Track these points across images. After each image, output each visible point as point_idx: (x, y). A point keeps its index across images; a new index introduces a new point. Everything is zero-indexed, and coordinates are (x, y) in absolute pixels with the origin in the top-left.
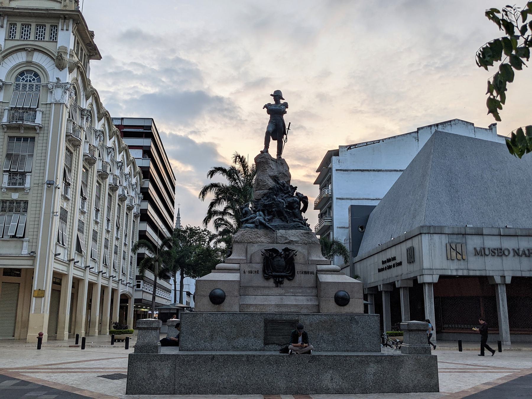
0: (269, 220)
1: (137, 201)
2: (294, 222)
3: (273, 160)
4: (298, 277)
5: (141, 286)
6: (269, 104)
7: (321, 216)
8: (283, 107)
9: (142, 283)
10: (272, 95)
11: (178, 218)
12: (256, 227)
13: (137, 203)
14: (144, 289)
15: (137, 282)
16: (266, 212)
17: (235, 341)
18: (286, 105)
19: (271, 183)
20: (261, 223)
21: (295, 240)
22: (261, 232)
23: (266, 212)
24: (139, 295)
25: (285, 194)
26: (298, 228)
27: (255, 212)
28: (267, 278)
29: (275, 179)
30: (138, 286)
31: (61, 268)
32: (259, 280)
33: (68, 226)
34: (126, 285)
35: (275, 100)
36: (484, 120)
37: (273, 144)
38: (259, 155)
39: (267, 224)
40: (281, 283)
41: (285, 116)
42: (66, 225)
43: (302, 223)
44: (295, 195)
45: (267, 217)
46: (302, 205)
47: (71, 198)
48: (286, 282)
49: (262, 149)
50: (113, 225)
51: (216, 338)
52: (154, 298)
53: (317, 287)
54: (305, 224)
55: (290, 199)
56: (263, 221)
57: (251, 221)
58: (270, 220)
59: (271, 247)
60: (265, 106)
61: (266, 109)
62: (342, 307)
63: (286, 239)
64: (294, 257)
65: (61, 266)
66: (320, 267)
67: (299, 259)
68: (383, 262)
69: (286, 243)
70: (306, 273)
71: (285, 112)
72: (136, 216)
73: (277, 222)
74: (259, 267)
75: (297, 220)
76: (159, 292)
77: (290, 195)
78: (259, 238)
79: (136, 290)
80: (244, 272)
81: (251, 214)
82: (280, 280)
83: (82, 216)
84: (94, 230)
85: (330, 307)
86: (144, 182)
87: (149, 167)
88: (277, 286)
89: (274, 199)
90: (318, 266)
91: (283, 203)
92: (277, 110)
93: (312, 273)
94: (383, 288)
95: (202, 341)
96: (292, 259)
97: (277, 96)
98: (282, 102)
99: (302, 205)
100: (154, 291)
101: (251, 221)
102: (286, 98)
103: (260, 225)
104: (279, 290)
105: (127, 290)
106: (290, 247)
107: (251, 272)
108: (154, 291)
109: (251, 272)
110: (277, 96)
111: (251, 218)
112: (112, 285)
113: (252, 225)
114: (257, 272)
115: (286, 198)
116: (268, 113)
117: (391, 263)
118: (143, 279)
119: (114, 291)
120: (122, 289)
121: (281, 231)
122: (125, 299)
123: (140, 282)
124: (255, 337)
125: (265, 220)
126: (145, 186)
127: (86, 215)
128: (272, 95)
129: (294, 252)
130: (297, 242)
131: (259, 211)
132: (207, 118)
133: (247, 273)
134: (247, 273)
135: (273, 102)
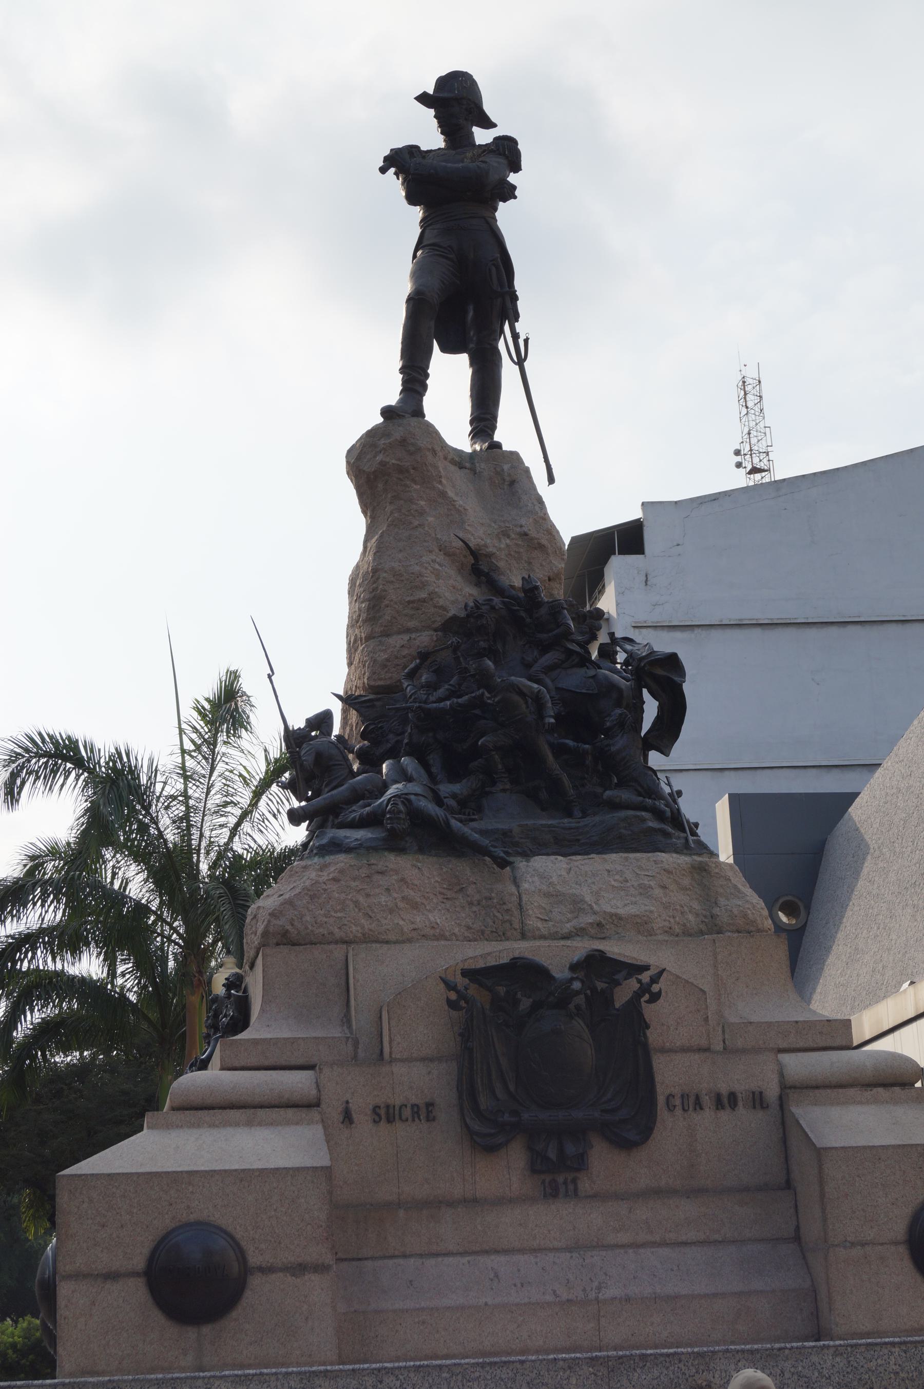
0: (463, 803)
2: (615, 806)
3: (458, 459)
4: (670, 1129)
6: (413, 150)
8: (494, 161)
10: (424, 99)
12: (394, 843)
18: (508, 152)
19: (454, 593)
20: (418, 819)
21: (632, 910)
22: (417, 872)
23: (434, 759)
25: (545, 649)
26: (647, 842)
27: (370, 761)
28: (485, 1139)
29: (478, 566)
35: (447, 125)
36: (639, 977)
37: (450, 373)
38: (372, 434)
39: (455, 823)
40: (580, 1164)
41: (506, 215)
44: (594, 655)
45: (445, 789)
46: (651, 708)
48: (604, 1164)
53: (788, 1185)
54: (677, 820)
55: (574, 679)
56: (427, 806)
57: (357, 811)
58: (470, 806)
59: (497, 952)
63: (577, 905)
64: (649, 1011)
66: (798, 1065)
67: (668, 1021)
70: (726, 1101)
71: (509, 193)
73: (506, 814)
74: (420, 1077)
75: (625, 795)
77: (570, 653)
78: (415, 906)
80: (348, 1117)
81: (353, 775)
82: (570, 1149)
88: (552, 1193)
89: (484, 680)
90: (786, 1058)
91: (336, 912)
92: (458, 180)
93: (758, 1100)
96: (633, 1021)
97: (455, 100)
98: (482, 137)
99: (651, 708)
101: (357, 811)
102: (504, 112)
104: (554, 1220)
107: (386, 1114)
109: (386, 1114)
110: (455, 100)
111: (357, 796)
114: (425, 1112)
121: (540, 863)
128: (424, 99)
129: (645, 977)
131: (393, 754)
133: (363, 1120)
134: (363, 1120)
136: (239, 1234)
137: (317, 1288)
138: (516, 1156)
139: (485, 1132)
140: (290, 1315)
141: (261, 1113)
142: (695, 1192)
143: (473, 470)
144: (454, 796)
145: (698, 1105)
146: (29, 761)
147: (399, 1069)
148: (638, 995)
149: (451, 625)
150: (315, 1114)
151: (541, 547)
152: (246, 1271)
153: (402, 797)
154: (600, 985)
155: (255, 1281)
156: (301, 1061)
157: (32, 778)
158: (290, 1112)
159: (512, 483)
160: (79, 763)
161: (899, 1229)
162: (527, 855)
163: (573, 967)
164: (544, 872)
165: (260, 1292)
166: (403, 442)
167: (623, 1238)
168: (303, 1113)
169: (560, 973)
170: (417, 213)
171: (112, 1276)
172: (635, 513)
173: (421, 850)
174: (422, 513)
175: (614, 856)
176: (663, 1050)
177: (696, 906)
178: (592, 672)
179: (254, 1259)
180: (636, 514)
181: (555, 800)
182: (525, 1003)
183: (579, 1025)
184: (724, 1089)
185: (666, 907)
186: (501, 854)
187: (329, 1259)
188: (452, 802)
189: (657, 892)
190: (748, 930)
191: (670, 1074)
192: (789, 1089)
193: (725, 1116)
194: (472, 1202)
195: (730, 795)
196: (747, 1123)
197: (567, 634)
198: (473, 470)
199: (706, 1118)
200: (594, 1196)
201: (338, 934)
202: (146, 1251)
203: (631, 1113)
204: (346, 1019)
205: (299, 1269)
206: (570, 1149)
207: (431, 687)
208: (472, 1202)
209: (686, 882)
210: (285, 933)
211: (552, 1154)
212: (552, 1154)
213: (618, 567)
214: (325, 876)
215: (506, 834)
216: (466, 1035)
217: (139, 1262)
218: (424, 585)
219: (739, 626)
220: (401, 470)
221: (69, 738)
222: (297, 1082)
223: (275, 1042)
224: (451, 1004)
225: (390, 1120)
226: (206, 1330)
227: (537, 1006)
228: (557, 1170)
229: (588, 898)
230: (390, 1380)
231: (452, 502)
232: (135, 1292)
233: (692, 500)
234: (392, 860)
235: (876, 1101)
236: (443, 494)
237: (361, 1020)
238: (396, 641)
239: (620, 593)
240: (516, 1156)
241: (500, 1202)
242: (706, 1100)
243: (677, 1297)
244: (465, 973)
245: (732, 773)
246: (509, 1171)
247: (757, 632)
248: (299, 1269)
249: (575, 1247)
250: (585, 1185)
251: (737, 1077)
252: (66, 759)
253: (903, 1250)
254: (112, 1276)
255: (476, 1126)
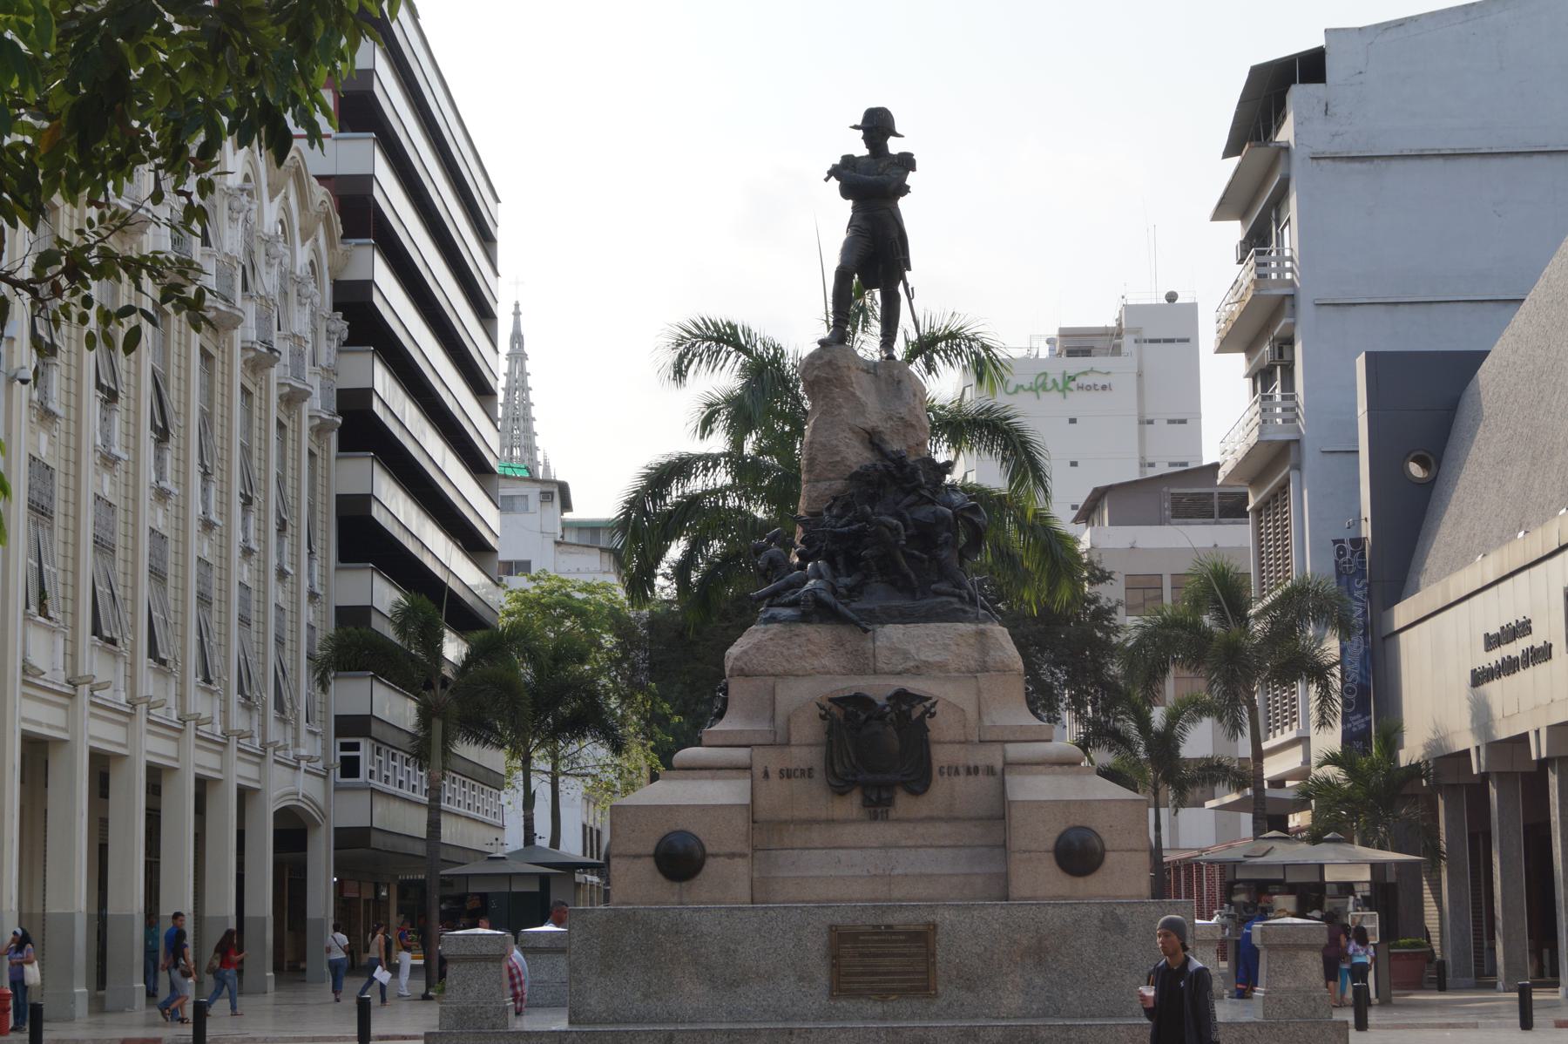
1: (327, 351)
2: (938, 594)
4: (940, 787)
5: (364, 767)
6: (848, 161)
7: (1262, 377)
9: (365, 751)
11: (517, 337)
12: (805, 618)
13: (319, 361)
14: (375, 783)
15: (344, 747)
16: (840, 559)
17: (740, 991)
18: (906, 162)
19: (857, 456)
20: (819, 603)
21: (938, 658)
22: (818, 635)
23: (840, 559)
24: (352, 812)
29: (873, 440)
30: (350, 767)
31: (45, 718)
32: (812, 798)
33: (59, 533)
34: (297, 768)
35: (868, 140)
39: (840, 607)
40: (890, 802)
41: (903, 203)
42: (51, 529)
43: (961, 598)
45: (844, 580)
47: (61, 411)
48: (903, 803)
49: (824, 333)
50: (225, 493)
51: (680, 983)
52: (434, 826)
55: (923, 513)
56: (826, 596)
58: (854, 592)
60: (835, 172)
61: (835, 183)
62: (1080, 881)
63: (906, 655)
65: (45, 707)
66: (1015, 751)
67: (942, 727)
68: (1492, 642)
69: (907, 671)
70: (973, 771)
72: (319, 430)
73: (878, 597)
74: (805, 754)
75: (944, 586)
76: (455, 794)
77: (922, 496)
78: (815, 655)
79: (338, 788)
80: (766, 775)
82: (885, 795)
83: (107, 478)
84: (152, 531)
85: (1040, 877)
86: (347, 257)
87: (368, 180)
88: (874, 818)
90: (1009, 747)
91: (897, 528)
93: (990, 771)
94: (1487, 760)
95: (638, 995)
96: (920, 729)
97: (877, 125)
100: (435, 793)
103: (818, 611)
105: (305, 788)
106: (915, 685)
107: (786, 774)
108: (435, 793)
109: (786, 774)
110: (877, 125)
112: (241, 772)
113: (788, 612)
115: (908, 507)
116: (846, 192)
117: (1515, 649)
118: (367, 734)
119: (244, 795)
120: (282, 787)
122: (292, 832)
123: (356, 747)
124: (801, 979)
125: (835, 592)
126: (354, 274)
127: (121, 466)
128: (855, 127)
129: (928, 704)
130: (942, 667)
132: (589, 739)
133: (774, 776)
134: (774, 776)
135: (861, 150)
136: (701, 837)
137: (741, 866)
138: (855, 798)
139: (840, 786)
140: (726, 880)
141: (720, 773)
142: (951, 819)
143: (875, 374)
144: (846, 586)
145: (957, 772)
146: (693, 345)
147: (795, 750)
148: (923, 714)
149: (855, 477)
150: (748, 774)
151: (913, 426)
152: (704, 856)
153: (813, 591)
154: (904, 707)
155: (710, 861)
156: (744, 742)
157: (697, 360)
158: (734, 773)
159: (899, 382)
160: (739, 347)
161: (1051, 844)
162: (883, 623)
163: (889, 699)
164: (892, 635)
165: (711, 866)
166: (830, 363)
167: (910, 843)
168: (741, 773)
169: (881, 702)
170: (850, 203)
171: (638, 856)
172: (1316, 41)
173: (821, 622)
174: (840, 407)
175: (932, 625)
176: (939, 743)
177: (976, 655)
178: (933, 509)
179: (709, 850)
180: (1318, 41)
181: (907, 589)
182: (863, 717)
183: (890, 729)
184: (972, 764)
185: (958, 656)
186: (864, 623)
187: (748, 851)
188: (843, 591)
189: (954, 648)
190: (1004, 670)
191: (941, 756)
192: (1008, 764)
193: (971, 778)
194: (831, 821)
195: (1367, 354)
196: (983, 782)
197: (920, 486)
198: (875, 374)
199: (960, 781)
200: (899, 820)
201: (771, 671)
202: (655, 843)
203: (919, 777)
204: (773, 719)
205: (732, 856)
206: (885, 795)
207: (839, 517)
208: (831, 821)
209: (972, 641)
210: (742, 670)
211: (874, 798)
212: (874, 798)
213: (1298, 94)
214: (767, 636)
215: (871, 611)
216: (829, 732)
217: (651, 850)
218: (838, 453)
219: (1420, 156)
220: (828, 380)
221: (729, 324)
222: (740, 755)
223: (731, 732)
224: (822, 717)
225: (789, 777)
226: (684, 884)
227: (869, 718)
228: (877, 805)
229: (913, 651)
230: (771, 913)
231: (858, 399)
232: (650, 864)
233: (1377, 26)
234: (804, 628)
235: (1054, 773)
236: (853, 394)
237: (780, 720)
238: (823, 486)
239: (1299, 123)
240: (855, 798)
241: (845, 822)
242: (961, 770)
243: (932, 875)
244: (831, 700)
245: (1407, 307)
246: (851, 805)
247: (1440, 161)
248: (732, 856)
249: (885, 847)
250: (893, 814)
251: (982, 757)
252: (728, 343)
253: (1051, 855)
254: (638, 856)
255: (834, 782)
